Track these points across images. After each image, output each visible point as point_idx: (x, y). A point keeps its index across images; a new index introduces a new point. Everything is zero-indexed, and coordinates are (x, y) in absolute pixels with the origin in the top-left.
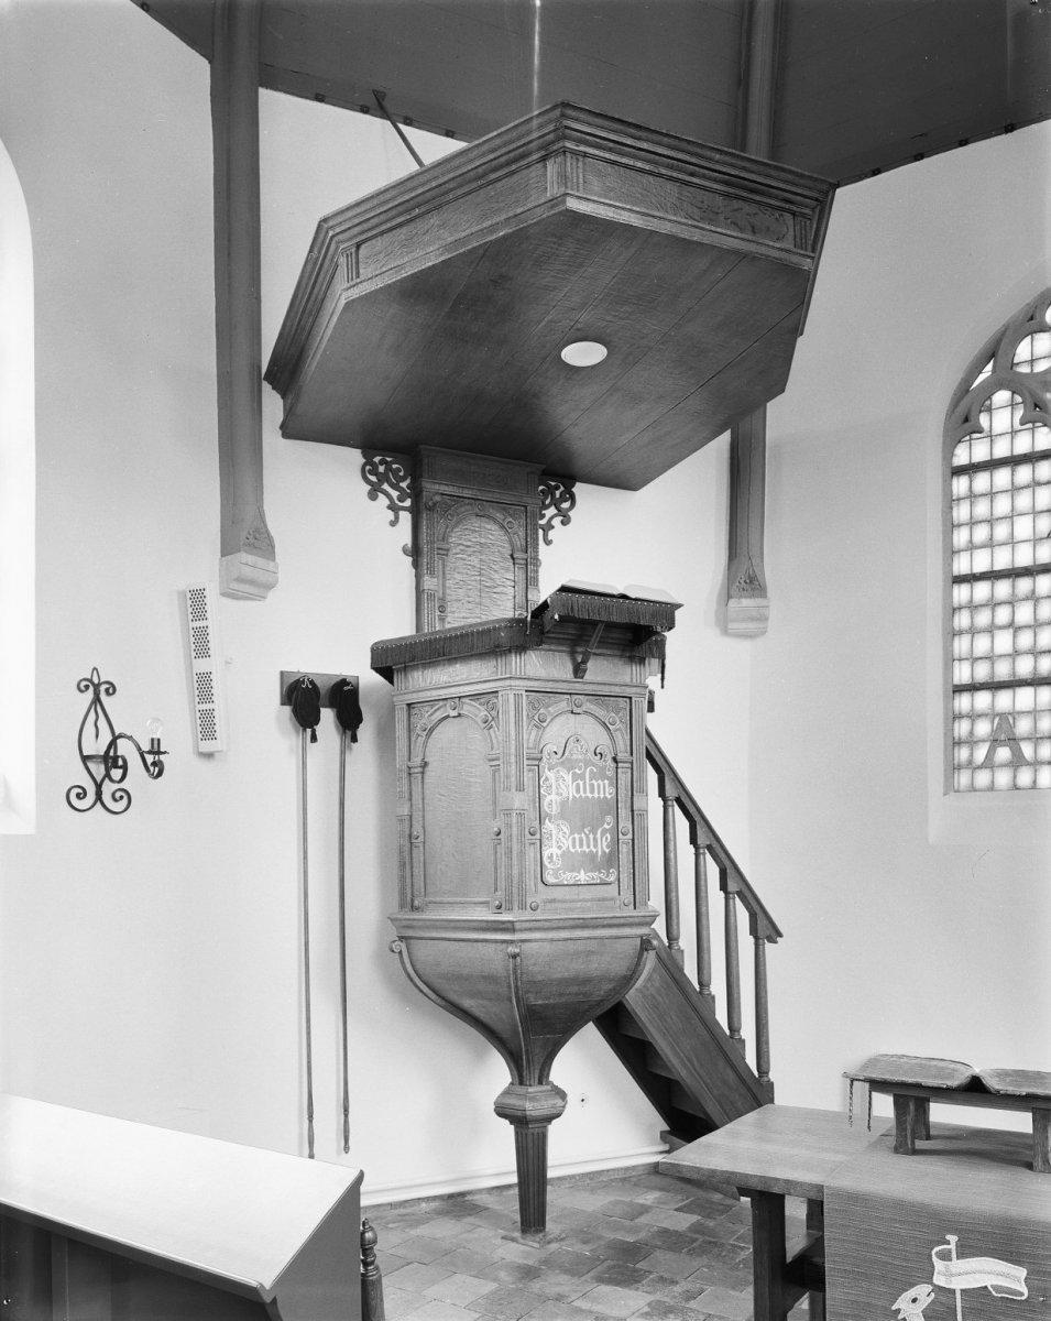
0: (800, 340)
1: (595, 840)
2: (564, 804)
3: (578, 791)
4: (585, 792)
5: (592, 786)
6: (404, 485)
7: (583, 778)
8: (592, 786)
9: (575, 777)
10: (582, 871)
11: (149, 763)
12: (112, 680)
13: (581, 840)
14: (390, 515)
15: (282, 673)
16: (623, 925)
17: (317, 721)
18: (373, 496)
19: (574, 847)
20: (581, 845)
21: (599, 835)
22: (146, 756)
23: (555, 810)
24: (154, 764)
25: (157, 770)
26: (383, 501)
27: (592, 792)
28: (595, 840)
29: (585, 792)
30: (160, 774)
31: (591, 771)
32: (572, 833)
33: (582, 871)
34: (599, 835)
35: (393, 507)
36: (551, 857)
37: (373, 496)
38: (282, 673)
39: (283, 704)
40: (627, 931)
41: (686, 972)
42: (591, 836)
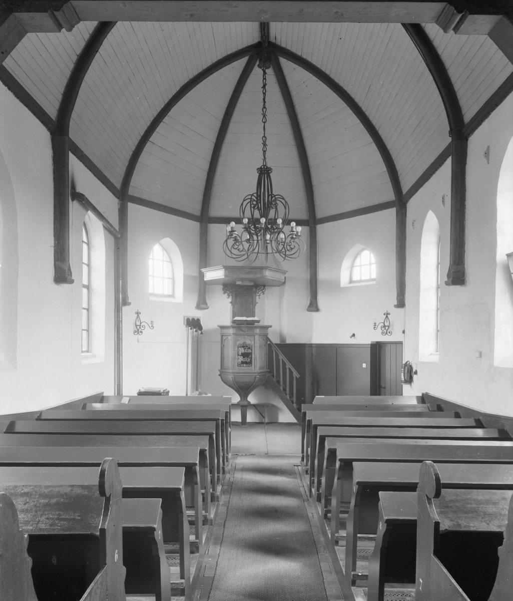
18: (224, 293)
23: (240, 354)
35: (228, 295)
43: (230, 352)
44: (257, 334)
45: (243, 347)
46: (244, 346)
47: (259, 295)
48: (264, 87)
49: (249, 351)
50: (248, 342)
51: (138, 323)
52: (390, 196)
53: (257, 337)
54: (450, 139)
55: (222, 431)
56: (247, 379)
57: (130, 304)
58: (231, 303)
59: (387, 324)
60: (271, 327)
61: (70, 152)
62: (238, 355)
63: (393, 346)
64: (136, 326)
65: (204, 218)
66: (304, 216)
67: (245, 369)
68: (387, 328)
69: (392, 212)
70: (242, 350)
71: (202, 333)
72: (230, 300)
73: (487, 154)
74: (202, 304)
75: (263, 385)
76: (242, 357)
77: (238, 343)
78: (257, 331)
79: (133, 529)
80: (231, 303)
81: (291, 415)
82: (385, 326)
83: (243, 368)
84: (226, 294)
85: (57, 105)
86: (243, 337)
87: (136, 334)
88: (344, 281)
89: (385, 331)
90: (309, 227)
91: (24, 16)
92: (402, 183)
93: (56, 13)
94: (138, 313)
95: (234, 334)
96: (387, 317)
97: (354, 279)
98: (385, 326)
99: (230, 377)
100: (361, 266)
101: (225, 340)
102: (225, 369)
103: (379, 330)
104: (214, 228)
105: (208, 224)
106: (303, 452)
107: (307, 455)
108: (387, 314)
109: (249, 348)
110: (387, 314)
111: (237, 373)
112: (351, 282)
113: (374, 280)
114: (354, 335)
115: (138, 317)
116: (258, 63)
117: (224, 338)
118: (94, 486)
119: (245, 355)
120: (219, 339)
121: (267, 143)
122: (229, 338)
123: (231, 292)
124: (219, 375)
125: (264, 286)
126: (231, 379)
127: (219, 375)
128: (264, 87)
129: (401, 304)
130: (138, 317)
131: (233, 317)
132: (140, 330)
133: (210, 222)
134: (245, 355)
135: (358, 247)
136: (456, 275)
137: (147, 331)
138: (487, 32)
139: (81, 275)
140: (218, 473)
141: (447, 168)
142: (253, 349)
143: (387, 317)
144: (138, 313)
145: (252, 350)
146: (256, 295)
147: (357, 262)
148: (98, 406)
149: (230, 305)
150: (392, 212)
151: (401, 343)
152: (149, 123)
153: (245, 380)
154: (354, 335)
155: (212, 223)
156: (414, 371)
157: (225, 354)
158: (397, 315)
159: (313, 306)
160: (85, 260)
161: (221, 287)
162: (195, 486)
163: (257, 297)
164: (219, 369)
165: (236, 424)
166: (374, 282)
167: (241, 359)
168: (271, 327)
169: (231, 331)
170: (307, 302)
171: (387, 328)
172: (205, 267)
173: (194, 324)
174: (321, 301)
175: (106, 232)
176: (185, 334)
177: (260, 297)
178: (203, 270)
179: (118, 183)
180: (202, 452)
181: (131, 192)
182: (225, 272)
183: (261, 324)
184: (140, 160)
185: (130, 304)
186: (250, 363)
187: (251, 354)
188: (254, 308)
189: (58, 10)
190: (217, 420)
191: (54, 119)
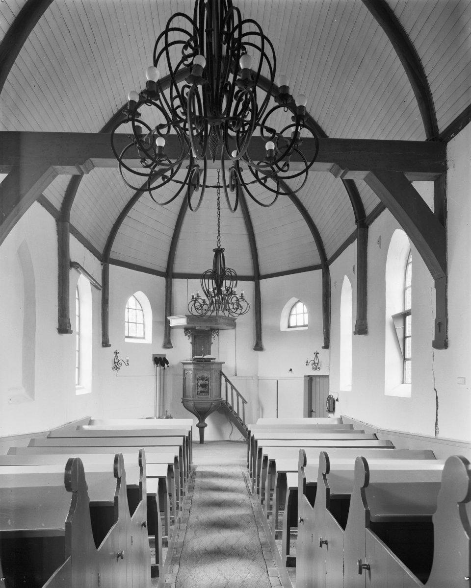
18: (186, 335)
35: (189, 337)
37: (186, 335)
43: (191, 383)
46: (202, 379)
48: (218, 199)
51: (116, 361)
52: (318, 261)
54: (355, 227)
55: (187, 446)
57: (110, 346)
59: (316, 362)
60: (224, 363)
61: (70, 234)
62: (198, 386)
63: (322, 380)
64: (115, 363)
65: (169, 274)
66: (249, 272)
67: (203, 397)
68: (316, 365)
69: (319, 273)
70: (201, 382)
71: (168, 366)
72: (190, 341)
73: (379, 242)
74: (168, 344)
75: (217, 410)
77: (197, 376)
79: (443, 164)
80: (191, 343)
81: (118, 133)
82: (315, 363)
83: (201, 396)
84: (187, 337)
85: (61, 200)
87: (114, 369)
88: (284, 327)
89: (315, 367)
90: (254, 282)
91: (59, 167)
92: (327, 252)
93: (81, 167)
94: (116, 353)
96: (316, 356)
97: (292, 325)
98: (315, 363)
99: (191, 404)
100: (296, 314)
102: (187, 397)
103: (310, 366)
104: (178, 283)
105: (173, 279)
106: (248, 461)
107: (263, 488)
108: (317, 354)
110: (317, 354)
112: (289, 327)
113: (307, 326)
114: (291, 370)
115: (116, 355)
117: (186, 372)
118: (111, 472)
119: (203, 386)
120: (182, 373)
121: (220, 208)
123: (192, 335)
125: (218, 330)
126: (192, 406)
128: (218, 199)
129: (327, 346)
130: (116, 355)
131: (193, 356)
132: (118, 366)
133: (174, 278)
134: (203, 386)
135: (294, 300)
136: (361, 328)
137: (123, 367)
138: (363, 178)
139: (75, 325)
140: (185, 476)
141: (354, 247)
143: (316, 356)
144: (116, 353)
147: (294, 312)
148: (86, 427)
149: (191, 344)
150: (319, 273)
151: (327, 377)
152: (126, 203)
153: (203, 406)
154: (291, 370)
155: (176, 278)
156: (335, 399)
157: (187, 385)
158: (323, 353)
159: (258, 347)
160: (77, 313)
161: (184, 330)
162: (172, 479)
163: (212, 339)
164: (182, 397)
165: (196, 443)
166: (307, 328)
167: (200, 389)
168: (224, 363)
169: (191, 367)
170: (252, 342)
171: (316, 365)
172: (170, 315)
173: (160, 361)
174: (265, 342)
175: (94, 287)
178: (169, 318)
179: (101, 249)
180: (176, 458)
181: (112, 256)
182: (187, 320)
183: (217, 361)
184: (119, 231)
185: (110, 346)
186: (208, 392)
187: (208, 385)
188: (210, 347)
189: (82, 164)
190: (184, 436)
191: (59, 210)
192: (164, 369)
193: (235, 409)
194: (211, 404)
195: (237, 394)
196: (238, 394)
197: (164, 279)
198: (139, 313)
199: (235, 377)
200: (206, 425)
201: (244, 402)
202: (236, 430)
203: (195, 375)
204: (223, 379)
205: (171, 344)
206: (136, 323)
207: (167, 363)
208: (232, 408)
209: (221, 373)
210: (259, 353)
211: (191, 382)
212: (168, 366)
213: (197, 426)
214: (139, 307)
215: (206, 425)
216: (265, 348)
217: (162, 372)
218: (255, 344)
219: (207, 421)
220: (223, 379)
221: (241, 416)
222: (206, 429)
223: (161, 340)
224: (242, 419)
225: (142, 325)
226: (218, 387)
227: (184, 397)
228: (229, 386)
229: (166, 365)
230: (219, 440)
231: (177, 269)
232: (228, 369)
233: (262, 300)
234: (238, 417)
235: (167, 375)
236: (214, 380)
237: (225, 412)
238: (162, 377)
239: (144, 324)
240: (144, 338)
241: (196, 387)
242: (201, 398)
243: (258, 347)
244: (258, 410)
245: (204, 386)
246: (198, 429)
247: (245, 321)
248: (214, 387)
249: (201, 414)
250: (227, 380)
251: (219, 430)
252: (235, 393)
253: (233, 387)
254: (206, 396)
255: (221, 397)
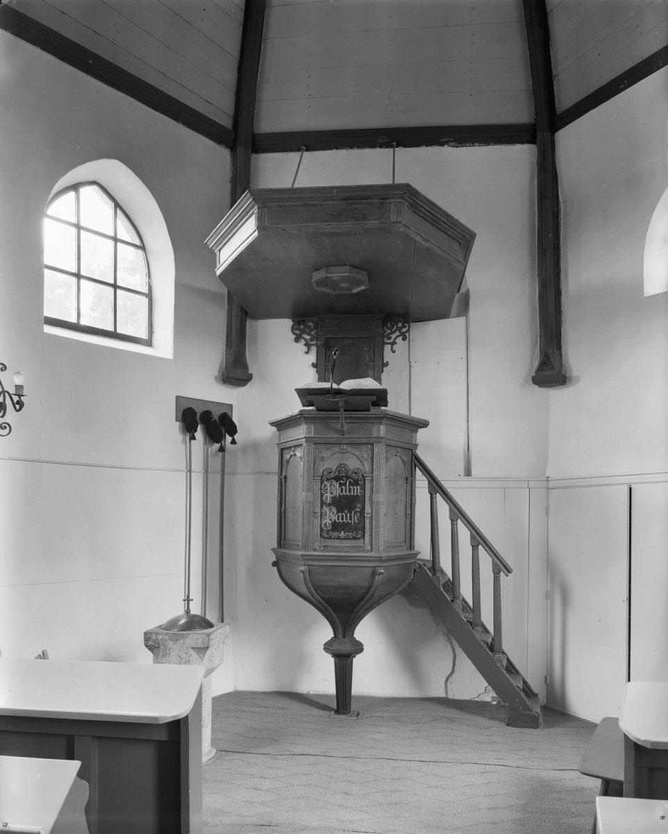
0: (335, 150)
1: (351, 516)
2: (334, 499)
3: (342, 492)
4: (346, 492)
5: (350, 489)
6: (313, 333)
7: (345, 484)
8: (350, 489)
9: (341, 485)
10: (342, 532)
11: (15, 401)
12: (6, 365)
13: (342, 516)
14: (305, 349)
15: (177, 397)
16: (363, 561)
17: (196, 431)
18: (297, 340)
19: (338, 519)
20: (342, 519)
21: (353, 515)
22: (13, 396)
23: (329, 501)
24: (18, 402)
25: (19, 405)
26: (303, 342)
27: (350, 492)
28: (351, 516)
29: (346, 492)
30: (20, 409)
31: (350, 482)
32: (338, 512)
33: (342, 532)
34: (353, 515)
35: (307, 345)
36: (325, 524)
37: (297, 340)
38: (177, 397)
39: (177, 420)
40: (366, 564)
41: (233, 419)
42: (348, 515)
44: (379, 440)
45: (337, 479)
46: (340, 476)
47: (394, 343)
49: (357, 490)
50: (352, 463)
53: (379, 449)
56: (356, 579)
58: (314, 365)
62: (322, 503)
67: (342, 546)
70: (334, 490)
71: (234, 442)
72: (312, 358)
74: (236, 372)
75: (404, 593)
76: (334, 510)
78: (382, 430)
80: (314, 365)
83: (337, 543)
84: (301, 346)
86: (336, 449)
90: (533, 147)
95: (308, 439)
101: (288, 462)
105: (254, 156)
109: (356, 483)
111: (319, 558)
116: (383, 408)
119: (342, 504)
122: (299, 453)
124: (274, 564)
127: (274, 564)
133: (257, 150)
134: (342, 504)
142: (368, 486)
145: (363, 488)
146: (384, 343)
153: (341, 580)
155: (264, 151)
157: (289, 501)
159: (550, 371)
163: (387, 348)
167: (331, 515)
170: (524, 356)
174: (575, 353)
176: (204, 448)
177: (395, 347)
183: (395, 406)
187: (360, 499)
192: (222, 449)
193: (466, 591)
194: (374, 574)
195: (472, 537)
196: (478, 539)
197: (224, 153)
198: (128, 254)
199: (467, 482)
200: (359, 648)
201: (501, 567)
202: (466, 666)
203: (315, 461)
204: (421, 483)
205: (247, 368)
206: (115, 286)
207: (232, 429)
208: (453, 586)
209: (416, 462)
210: (555, 395)
211: (300, 489)
212: (234, 442)
213: (328, 647)
214: (125, 232)
215: (359, 648)
216: (575, 374)
217: (215, 463)
218: (536, 364)
219: (367, 630)
220: (421, 483)
221: (487, 618)
222: (358, 662)
223: (214, 355)
224: (490, 626)
225: (145, 301)
226: (401, 509)
227: (280, 545)
228: (443, 508)
229: (229, 439)
230: (412, 696)
231: (270, 120)
232: (440, 445)
233: (562, 206)
234: (476, 623)
235: (233, 473)
236: (383, 482)
237: (425, 595)
238: (215, 479)
239: (149, 296)
240: (149, 343)
241: (318, 509)
242: (337, 549)
243: (550, 371)
244: (548, 595)
245: (349, 506)
246: (330, 661)
247: (497, 281)
248: (383, 509)
249: (343, 609)
250: (436, 487)
251: (411, 664)
252: (464, 534)
253: (457, 513)
254: (354, 543)
255: (411, 547)
